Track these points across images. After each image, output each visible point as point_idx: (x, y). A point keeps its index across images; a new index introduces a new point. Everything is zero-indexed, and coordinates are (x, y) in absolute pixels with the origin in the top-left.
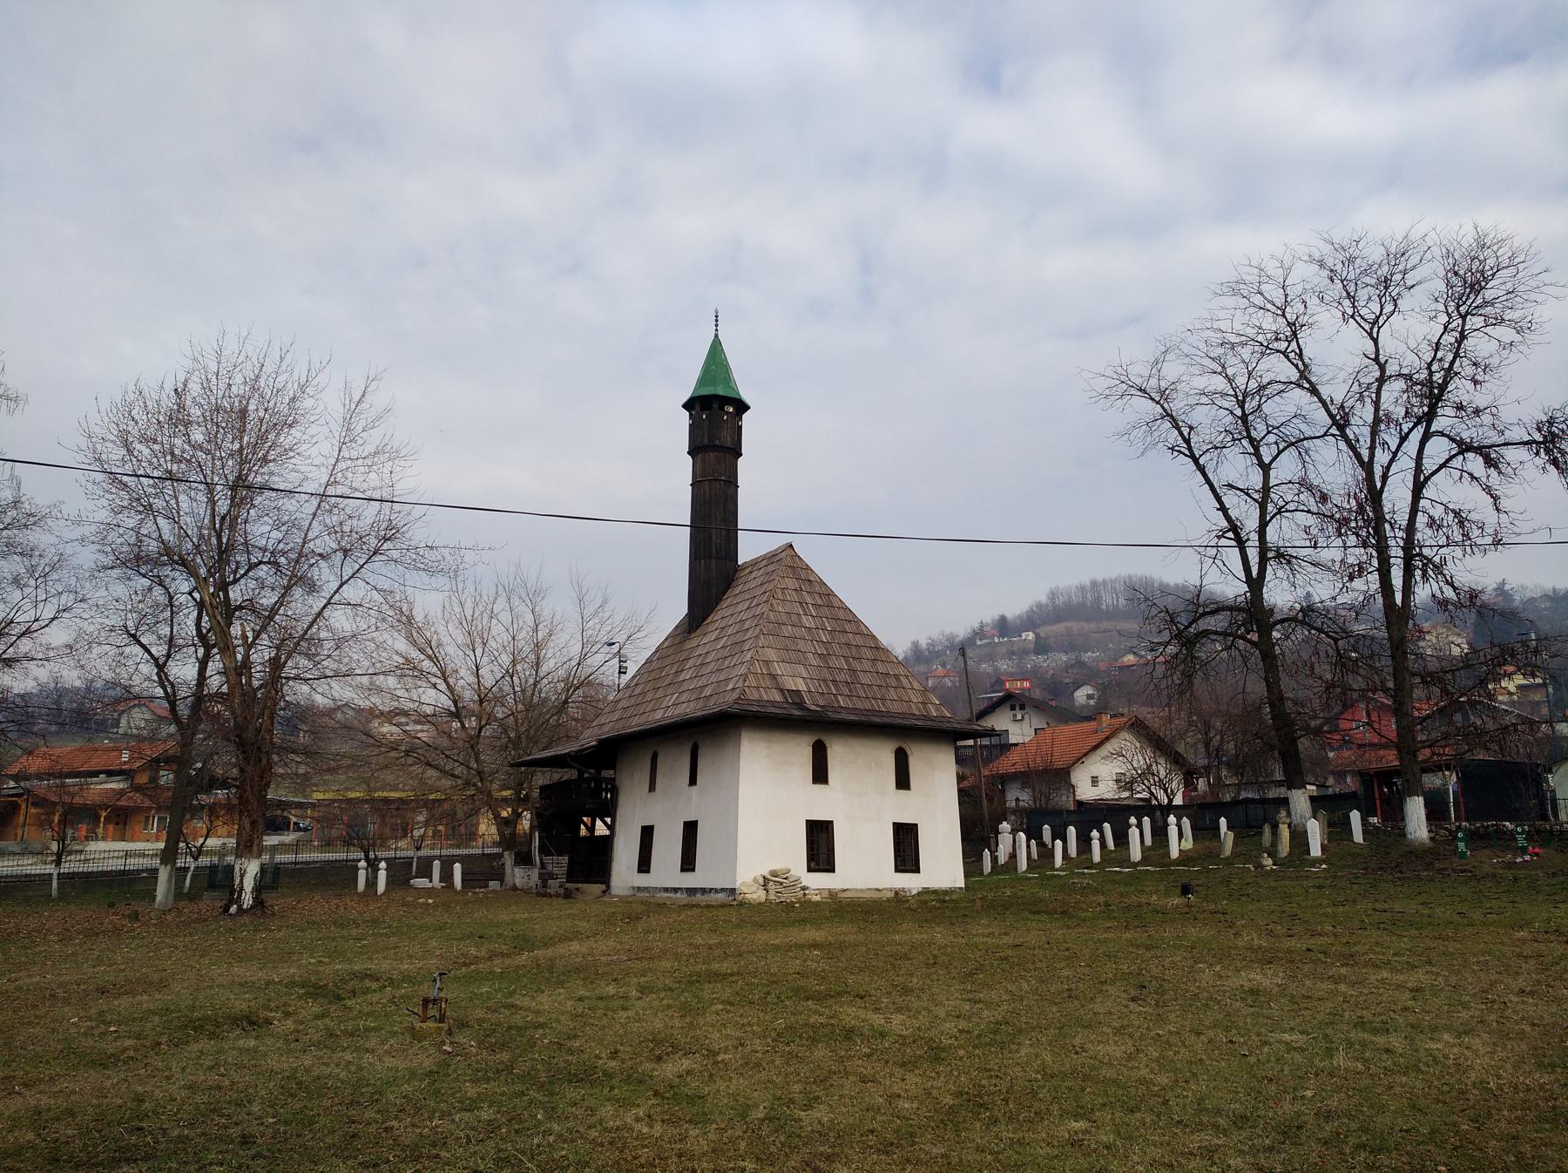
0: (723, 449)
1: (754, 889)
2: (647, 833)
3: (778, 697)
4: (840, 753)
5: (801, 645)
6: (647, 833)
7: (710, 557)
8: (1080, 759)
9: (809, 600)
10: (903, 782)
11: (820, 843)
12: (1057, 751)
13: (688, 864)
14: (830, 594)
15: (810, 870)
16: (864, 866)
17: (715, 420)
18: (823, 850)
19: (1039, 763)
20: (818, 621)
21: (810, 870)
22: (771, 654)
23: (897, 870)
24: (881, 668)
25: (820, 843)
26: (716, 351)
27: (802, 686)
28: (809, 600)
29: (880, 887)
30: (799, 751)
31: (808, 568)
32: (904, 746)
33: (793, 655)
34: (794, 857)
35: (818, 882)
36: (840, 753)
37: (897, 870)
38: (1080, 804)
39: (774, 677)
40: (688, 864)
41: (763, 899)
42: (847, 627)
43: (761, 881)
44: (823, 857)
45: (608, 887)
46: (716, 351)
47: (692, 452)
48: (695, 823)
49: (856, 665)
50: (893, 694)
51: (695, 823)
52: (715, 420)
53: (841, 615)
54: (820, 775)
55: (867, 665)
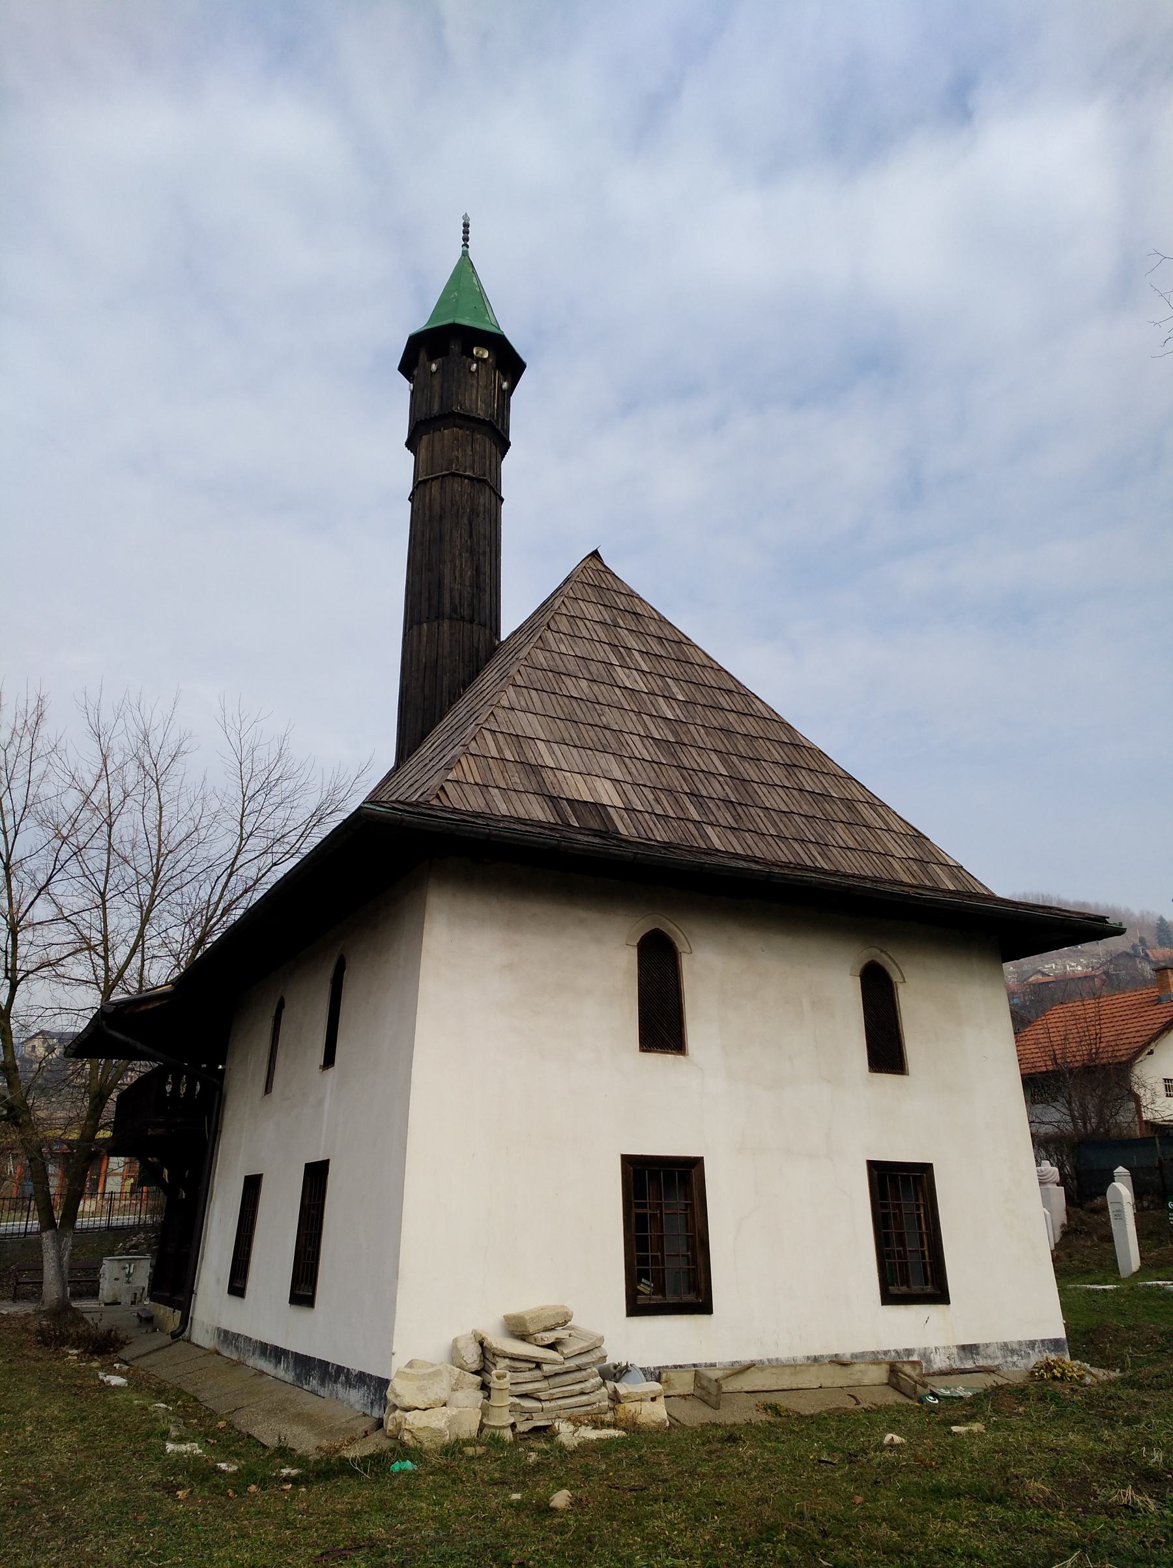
0: (467, 421)
1: (440, 1390)
2: (253, 1185)
3: (538, 811)
4: (713, 971)
5: (611, 718)
6: (253, 1185)
7: (439, 617)
8: (1144, 1048)
9: (632, 642)
10: (886, 1053)
11: (665, 1227)
12: (1108, 1034)
13: (303, 1291)
14: (682, 641)
15: (635, 1308)
16: (793, 1295)
17: (460, 380)
18: (676, 1246)
19: (1077, 1055)
20: (656, 684)
21: (635, 1308)
22: (530, 725)
23: (888, 1298)
24: (809, 782)
25: (665, 1227)
26: (465, 268)
27: (607, 794)
28: (632, 642)
29: (846, 1348)
30: (598, 964)
31: (631, 595)
32: (884, 960)
33: (590, 735)
34: (582, 1268)
35: (669, 1340)
36: (713, 971)
37: (888, 1298)
38: (1152, 1125)
39: (534, 769)
40: (303, 1291)
41: (469, 1426)
42: (724, 700)
43: (472, 1357)
44: (674, 1265)
45: (185, 1320)
46: (465, 268)
47: (412, 444)
48: (326, 1163)
49: (750, 771)
50: (842, 835)
51: (326, 1163)
52: (460, 380)
53: (709, 678)
54: (662, 1025)
55: (777, 775)
